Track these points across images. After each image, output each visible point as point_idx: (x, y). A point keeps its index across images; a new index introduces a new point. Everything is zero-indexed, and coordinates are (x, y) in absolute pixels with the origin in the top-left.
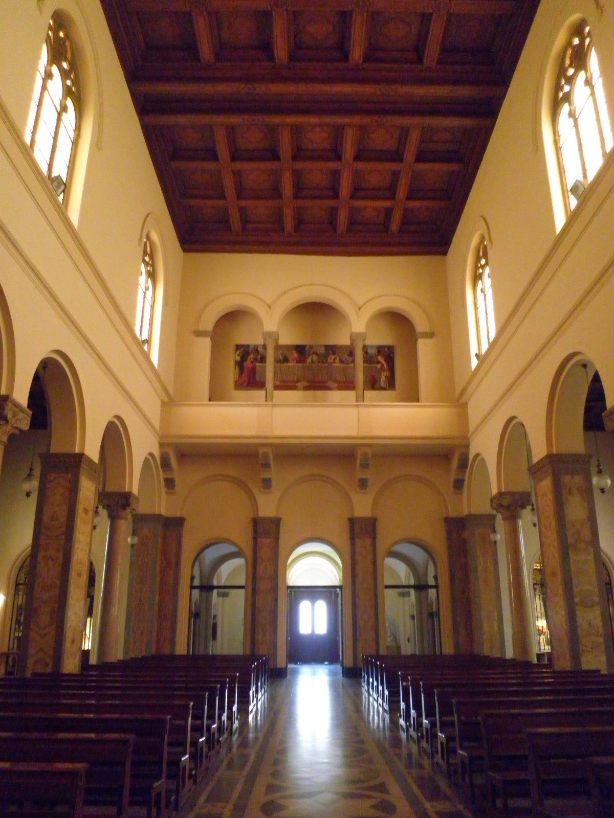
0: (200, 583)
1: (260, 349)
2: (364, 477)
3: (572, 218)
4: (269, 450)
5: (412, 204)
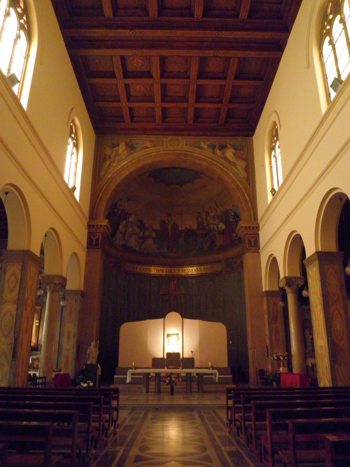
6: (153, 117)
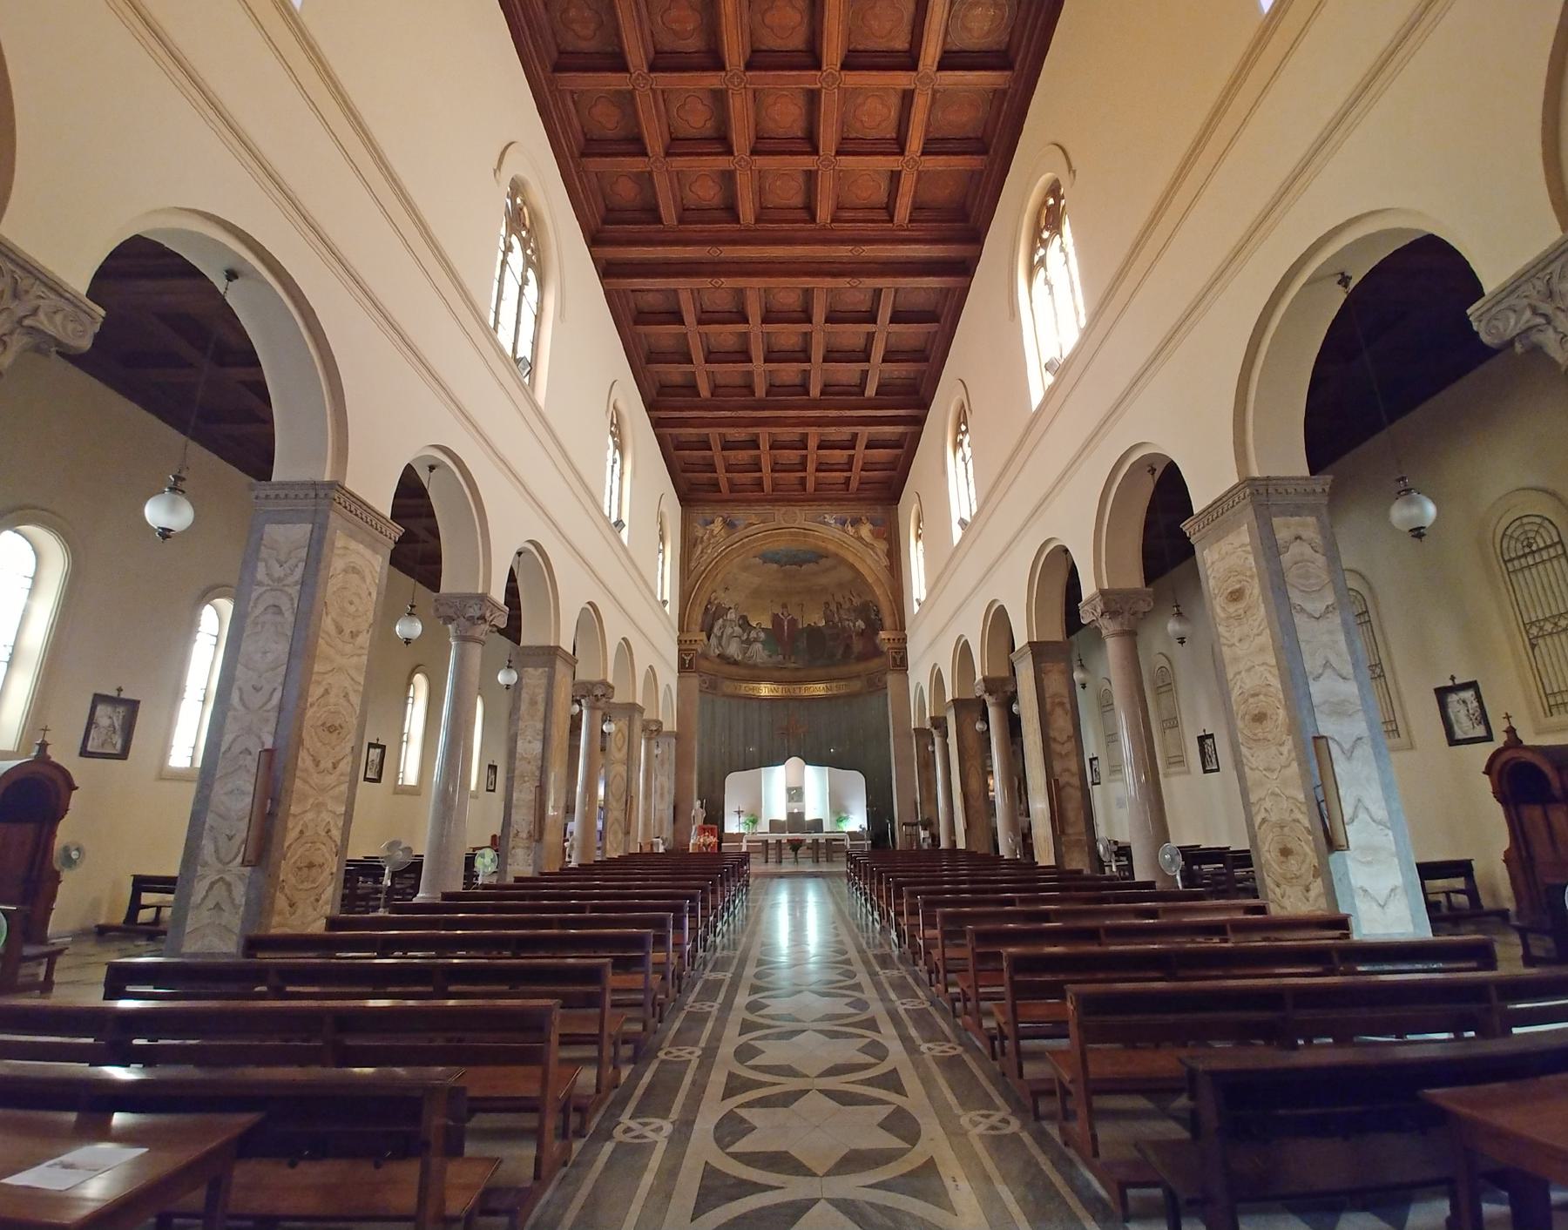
3: (1050, 393)
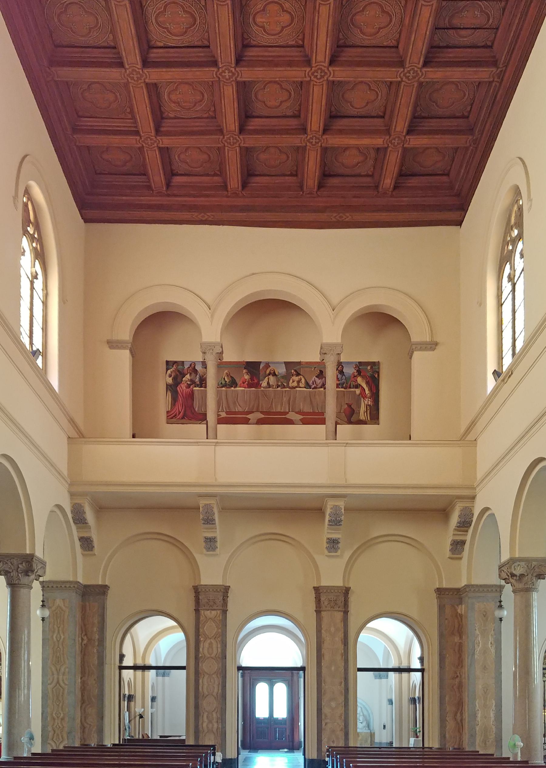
0: (134, 664)
1: (199, 368)
2: (334, 536)
4: (212, 501)
5: (415, 141)
6: (221, 172)
